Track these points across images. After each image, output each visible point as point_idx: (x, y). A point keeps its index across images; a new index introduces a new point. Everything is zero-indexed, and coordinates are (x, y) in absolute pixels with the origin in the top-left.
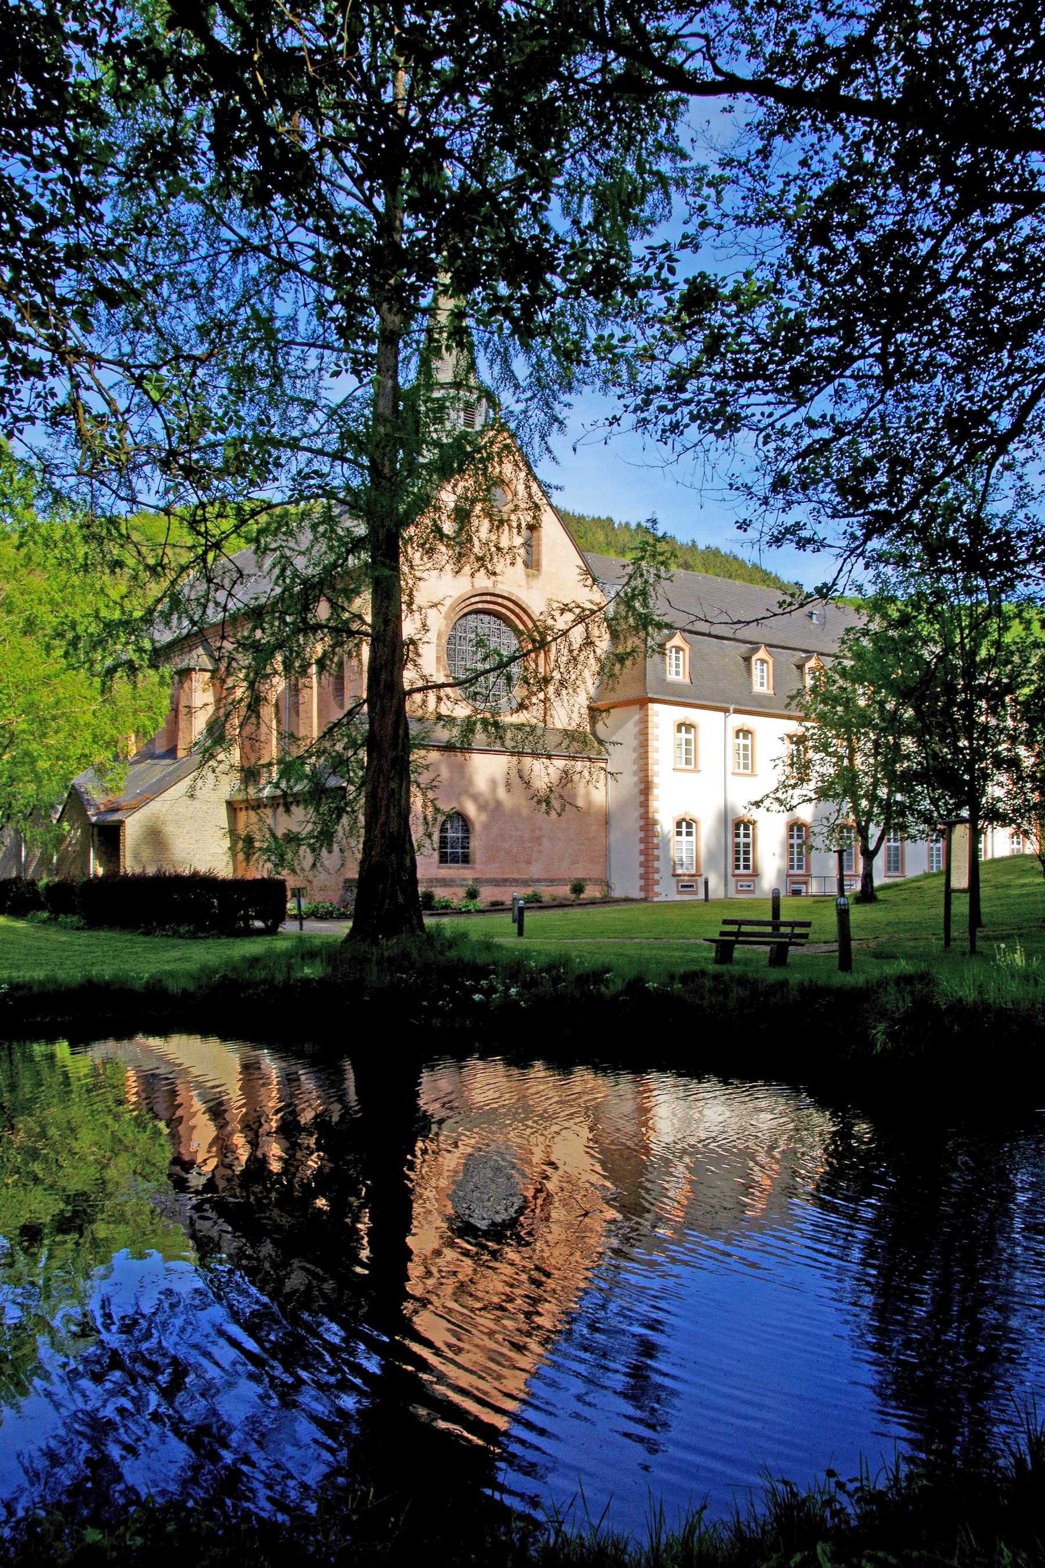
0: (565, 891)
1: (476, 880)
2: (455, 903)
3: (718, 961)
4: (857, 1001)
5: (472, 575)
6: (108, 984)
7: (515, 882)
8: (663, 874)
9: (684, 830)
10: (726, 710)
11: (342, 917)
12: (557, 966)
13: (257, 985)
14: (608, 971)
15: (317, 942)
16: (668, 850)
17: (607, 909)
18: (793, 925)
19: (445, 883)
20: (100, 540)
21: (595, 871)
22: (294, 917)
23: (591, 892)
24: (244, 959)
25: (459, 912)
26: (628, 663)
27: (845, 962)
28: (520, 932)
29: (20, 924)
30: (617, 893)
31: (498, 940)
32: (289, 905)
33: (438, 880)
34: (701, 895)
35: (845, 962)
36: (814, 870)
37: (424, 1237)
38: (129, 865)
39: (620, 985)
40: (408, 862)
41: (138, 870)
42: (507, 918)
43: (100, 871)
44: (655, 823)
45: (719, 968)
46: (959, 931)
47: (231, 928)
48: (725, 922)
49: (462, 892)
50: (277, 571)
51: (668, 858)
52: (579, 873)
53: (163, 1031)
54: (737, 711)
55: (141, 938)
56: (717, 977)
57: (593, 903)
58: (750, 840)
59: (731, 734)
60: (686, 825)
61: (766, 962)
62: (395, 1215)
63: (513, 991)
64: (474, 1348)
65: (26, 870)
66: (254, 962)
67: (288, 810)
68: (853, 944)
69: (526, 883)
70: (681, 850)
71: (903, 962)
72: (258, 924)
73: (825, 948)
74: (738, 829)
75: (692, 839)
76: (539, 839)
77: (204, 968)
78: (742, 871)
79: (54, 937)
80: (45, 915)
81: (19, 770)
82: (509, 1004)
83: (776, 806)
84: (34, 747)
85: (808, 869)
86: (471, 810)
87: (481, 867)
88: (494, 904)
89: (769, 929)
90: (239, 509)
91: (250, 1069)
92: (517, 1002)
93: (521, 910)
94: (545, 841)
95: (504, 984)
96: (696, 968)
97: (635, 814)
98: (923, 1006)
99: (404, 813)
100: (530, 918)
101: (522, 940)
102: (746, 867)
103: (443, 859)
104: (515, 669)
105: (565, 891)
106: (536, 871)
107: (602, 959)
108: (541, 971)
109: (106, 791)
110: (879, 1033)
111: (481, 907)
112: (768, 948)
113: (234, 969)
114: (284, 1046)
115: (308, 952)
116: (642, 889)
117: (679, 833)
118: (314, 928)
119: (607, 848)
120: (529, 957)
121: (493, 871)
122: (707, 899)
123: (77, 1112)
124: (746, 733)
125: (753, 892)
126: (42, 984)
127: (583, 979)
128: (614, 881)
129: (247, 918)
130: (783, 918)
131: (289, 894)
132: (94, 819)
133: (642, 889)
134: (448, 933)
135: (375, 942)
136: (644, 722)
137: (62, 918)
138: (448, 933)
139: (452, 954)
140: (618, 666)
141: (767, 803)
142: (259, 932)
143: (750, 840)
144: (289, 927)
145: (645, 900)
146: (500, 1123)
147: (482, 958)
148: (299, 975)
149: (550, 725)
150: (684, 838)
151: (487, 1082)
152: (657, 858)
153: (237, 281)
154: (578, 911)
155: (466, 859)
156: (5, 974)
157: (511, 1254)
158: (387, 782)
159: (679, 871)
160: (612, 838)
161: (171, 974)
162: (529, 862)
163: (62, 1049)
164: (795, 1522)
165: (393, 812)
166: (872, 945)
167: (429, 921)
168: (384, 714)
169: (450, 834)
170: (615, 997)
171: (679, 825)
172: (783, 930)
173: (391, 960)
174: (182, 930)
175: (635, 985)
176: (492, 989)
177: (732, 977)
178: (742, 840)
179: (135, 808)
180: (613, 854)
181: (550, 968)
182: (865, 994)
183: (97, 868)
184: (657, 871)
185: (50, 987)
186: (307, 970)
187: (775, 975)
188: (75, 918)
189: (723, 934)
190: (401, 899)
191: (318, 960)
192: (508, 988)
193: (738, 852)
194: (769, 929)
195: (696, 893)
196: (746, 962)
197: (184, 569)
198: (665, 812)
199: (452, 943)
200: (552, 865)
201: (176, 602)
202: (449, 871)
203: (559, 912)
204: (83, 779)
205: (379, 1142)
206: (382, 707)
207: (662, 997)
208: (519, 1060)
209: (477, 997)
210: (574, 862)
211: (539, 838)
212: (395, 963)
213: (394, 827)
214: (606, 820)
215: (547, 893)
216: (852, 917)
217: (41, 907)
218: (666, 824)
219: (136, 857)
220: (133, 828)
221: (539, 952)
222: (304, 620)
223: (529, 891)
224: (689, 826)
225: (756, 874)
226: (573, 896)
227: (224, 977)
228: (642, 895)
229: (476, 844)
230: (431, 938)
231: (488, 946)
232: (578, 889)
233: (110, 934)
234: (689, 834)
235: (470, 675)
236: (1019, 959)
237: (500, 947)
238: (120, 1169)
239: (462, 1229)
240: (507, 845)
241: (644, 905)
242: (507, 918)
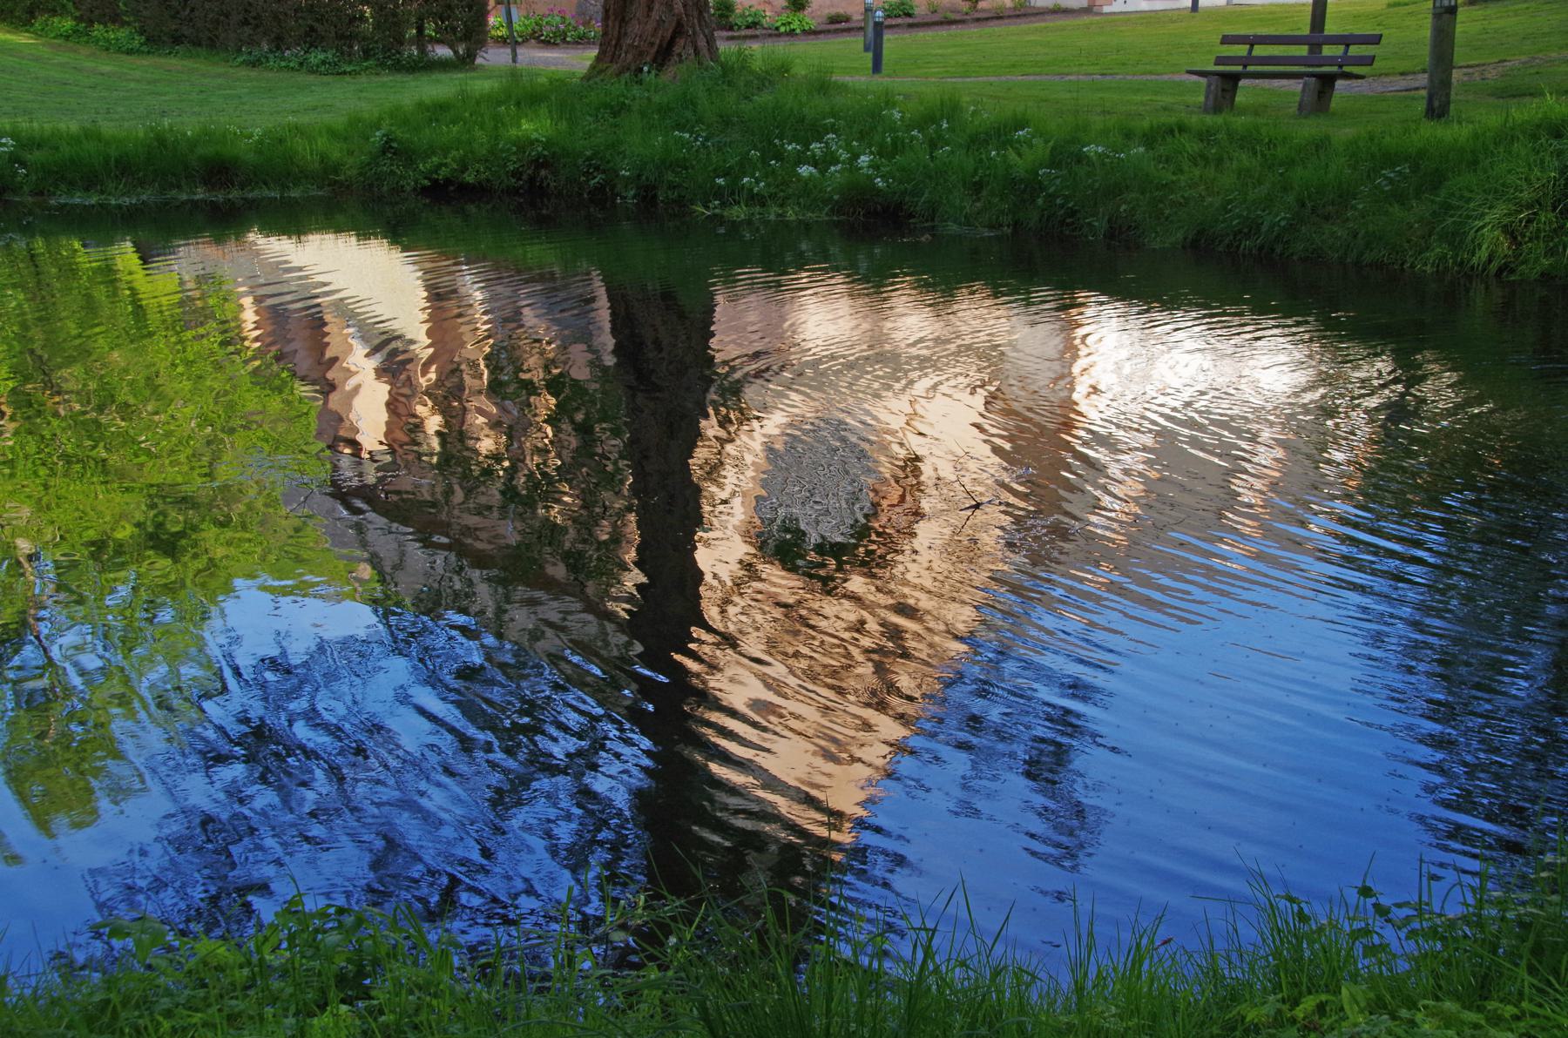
2: (769, 17)
6: (193, 144)
11: (581, 41)
12: (938, 118)
14: (1020, 125)
15: (542, 80)
18: (1346, 41)
22: (502, 41)
24: (420, 105)
25: (775, 34)
27: (1437, 109)
28: (877, 66)
29: (22, 39)
32: (492, 20)
35: (1437, 109)
37: (720, 553)
39: (1041, 150)
42: (856, 43)
45: (1210, 119)
48: (1226, 40)
55: (243, 72)
56: (1205, 136)
61: (1294, 109)
62: (675, 515)
63: (864, 160)
64: (795, 734)
66: (439, 110)
68: (1456, 74)
71: (1550, 99)
72: (443, 52)
73: (1403, 83)
77: (355, 121)
79: (89, 64)
80: (68, 24)
88: (835, 19)
89: (1303, 51)
92: (870, 178)
93: (879, 28)
95: (848, 148)
96: (1173, 120)
100: (892, 43)
101: (877, 79)
108: (909, 128)
111: (812, 24)
112: (1296, 86)
115: (529, 97)
118: (534, 57)
120: (890, 104)
123: (160, 350)
126: (74, 140)
130: (1331, 28)
137: (98, 30)
138: (757, 65)
139: (764, 98)
142: (443, 65)
144: (494, 58)
148: (513, 132)
149: (861, 350)
151: (823, 318)
154: (974, 30)
156: (6, 123)
157: (857, 583)
161: (298, 130)
163: (125, 256)
164: (1303, 967)
166: (1492, 74)
167: (725, 48)
172: (1327, 51)
173: (664, 110)
175: (1066, 155)
177: (1230, 135)
181: (927, 120)
182: (1472, 157)
187: (1309, 129)
188: (123, 33)
189: (1220, 61)
191: (543, 110)
192: (856, 157)
194: (1303, 51)
196: (1257, 111)
199: (765, 80)
203: (943, 32)
208: (872, 281)
209: (805, 170)
221: (907, 97)
230: (729, 73)
231: (823, 86)
233: (189, 63)
237: (843, 88)
239: (781, 545)
241: (1086, 19)
242: (856, 43)
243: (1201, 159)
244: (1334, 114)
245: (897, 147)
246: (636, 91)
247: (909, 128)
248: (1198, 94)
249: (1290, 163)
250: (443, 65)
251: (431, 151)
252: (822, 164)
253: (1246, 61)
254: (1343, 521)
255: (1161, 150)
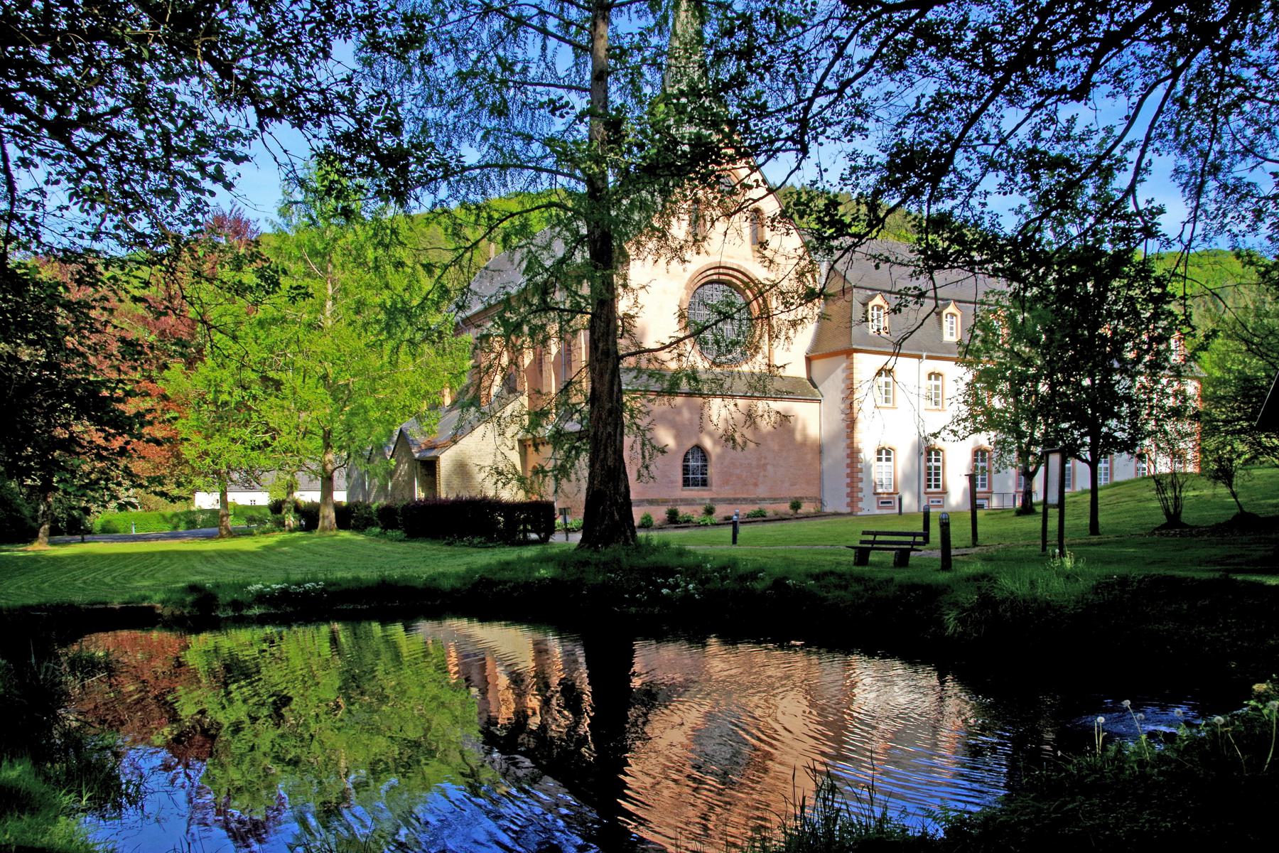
0: (785, 508)
1: (712, 499)
2: (696, 518)
3: (856, 564)
4: (930, 595)
5: (668, 263)
6: (397, 582)
7: (745, 500)
8: (866, 493)
9: (884, 456)
10: (920, 357)
13: (505, 582)
14: (762, 571)
16: (869, 474)
17: (818, 521)
19: (687, 502)
20: (387, 247)
21: (811, 491)
23: (806, 508)
24: (500, 563)
25: (698, 525)
26: (799, 328)
28: (734, 541)
29: (360, 538)
30: (828, 509)
31: (688, 548)
33: (682, 500)
34: (897, 510)
36: (995, 489)
38: (444, 493)
39: (768, 582)
40: (623, 489)
41: (452, 497)
43: (423, 495)
44: (859, 451)
46: (1052, 538)
47: (510, 537)
48: (864, 533)
49: (701, 509)
50: (524, 265)
51: (870, 481)
52: (797, 493)
53: (486, 617)
54: (928, 358)
57: (807, 517)
58: (939, 464)
59: (924, 376)
60: (885, 453)
63: (691, 586)
65: (369, 496)
66: (506, 565)
67: (537, 450)
69: (753, 501)
70: (881, 473)
72: (534, 536)
74: (928, 452)
75: (891, 464)
76: (765, 465)
77: (469, 570)
78: (933, 489)
80: (378, 530)
81: (355, 420)
82: (687, 595)
83: (951, 436)
84: (369, 402)
85: (990, 487)
86: (708, 443)
87: (716, 489)
90: (490, 218)
91: (541, 651)
94: (770, 468)
97: (843, 444)
98: (987, 601)
99: (619, 453)
100: (744, 530)
102: (937, 486)
103: (686, 482)
104: (708, 335)
105: (785, 508)
106: (761, 492)
107: (762, 560)
108: (714, 571)
109: (424, 433)
110: (951, 620)
113: (491, 570)
114: (563, 629)
116: (848, 505)
117: (879, 460)
119: (821, 473)
121: (727, 492)
122: (900, 512)
124: (938, 376)
125: (942, 506)
127: (742, 578)
128: (826, 499)
129: (525, 531)
131: (557, 512)
132: (417, 455)
133: (848, 505)
134: (655, 542)
135: (597, 550)
136: (850, 368)
137: (389, 532)
140: (792, 331)
141: (943, 434)
142: (534, 542)
143: (939, 464)
145: (850, 514)
146: (704, 693)
147: (674, 562)
150: (884, 463)
152: (861, 480)
153: (484, 36)
155: (704, 483)
158: (605, 427)
159: (880, 490)
160: (825, 464)
161: (444, 575)
162: (756, 485)
165: (610, 451)
168: (601, 375)
169: (692, 463)
170: (764, 592)
171: (879, 452)
173: (605, 564)
174: (476, 541)
175: (779, 583)
176: (677, 585)
178: (933, 464)
179: (445, 447)
180: (825, 477)
183: (420, 494)
184: (861, 490)
185: (353, 585)
186: (542, 572)
188: (398, 533)
189: (862, 542)
190: (617, 517)
192: (688, 584)
193: (929, 474)
195: (893, 508)
197: (447, 267)
198: (867, 441)
199: (656, 549)
200: (774, 487)
201: (445, 292)
202: (694, 493)
203: (778, 524)
204: (410, 425)
205: (618, 707)
206: (601, 369)
207: (801, 595)
209: (665, 591)
210: (793, 484)
211: (765, 465)
212: (606, 566)
213: (610, 462)
214: (820, 450)
215: (770, 509)
216: (952, 528)
217: (374, 525)
218: (868, 454)
219: (448, 485)
220: (446, 461)
222: (545, 301)
223: (756, 508)
224: (888, 453)
225: (945, 492)
226: (791, 512)
227: (482, 578)
228: (848, 510)
229: (712, 471)
230: (648, 548)
231: (681, 553)
232: (796, 506)
234: (888, 460)
235: (673, 340)
236: (1068, 563)
238: (441, 721)
240: (738, 472)
241: (848, 518)
243: (838, 587)
244: (912, 567)
245: (708, 580)
246: (595, 556)
247: (714, 571)
248: (850, 557)
249: (874, 589)
250: (534, 542)
251: (500, 582)
252: (673, 588)
253: (873, 542)
254: (823, 754)
255: (823, 582)
